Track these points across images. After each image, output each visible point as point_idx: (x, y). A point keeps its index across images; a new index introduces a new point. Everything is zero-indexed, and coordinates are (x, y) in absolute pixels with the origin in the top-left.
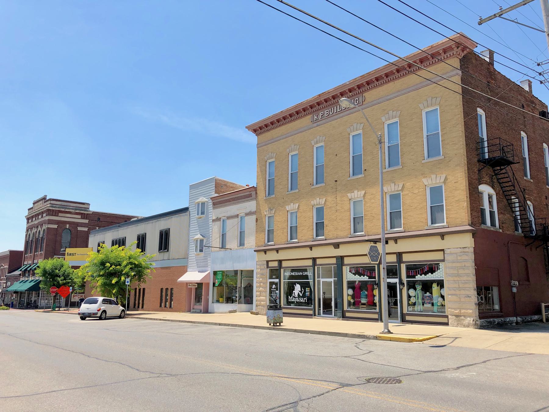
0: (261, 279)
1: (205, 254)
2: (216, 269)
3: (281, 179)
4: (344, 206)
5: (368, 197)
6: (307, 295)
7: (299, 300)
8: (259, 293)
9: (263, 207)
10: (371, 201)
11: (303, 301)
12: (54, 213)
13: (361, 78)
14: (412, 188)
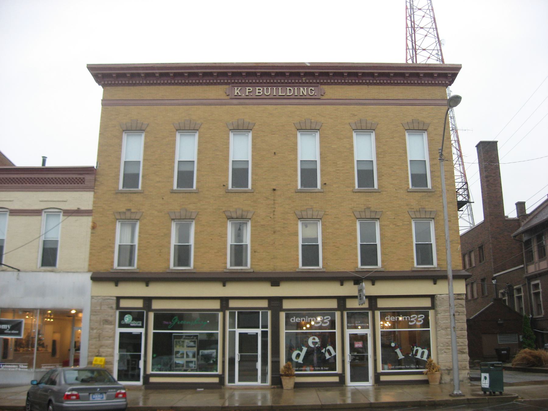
14: (394, 219)
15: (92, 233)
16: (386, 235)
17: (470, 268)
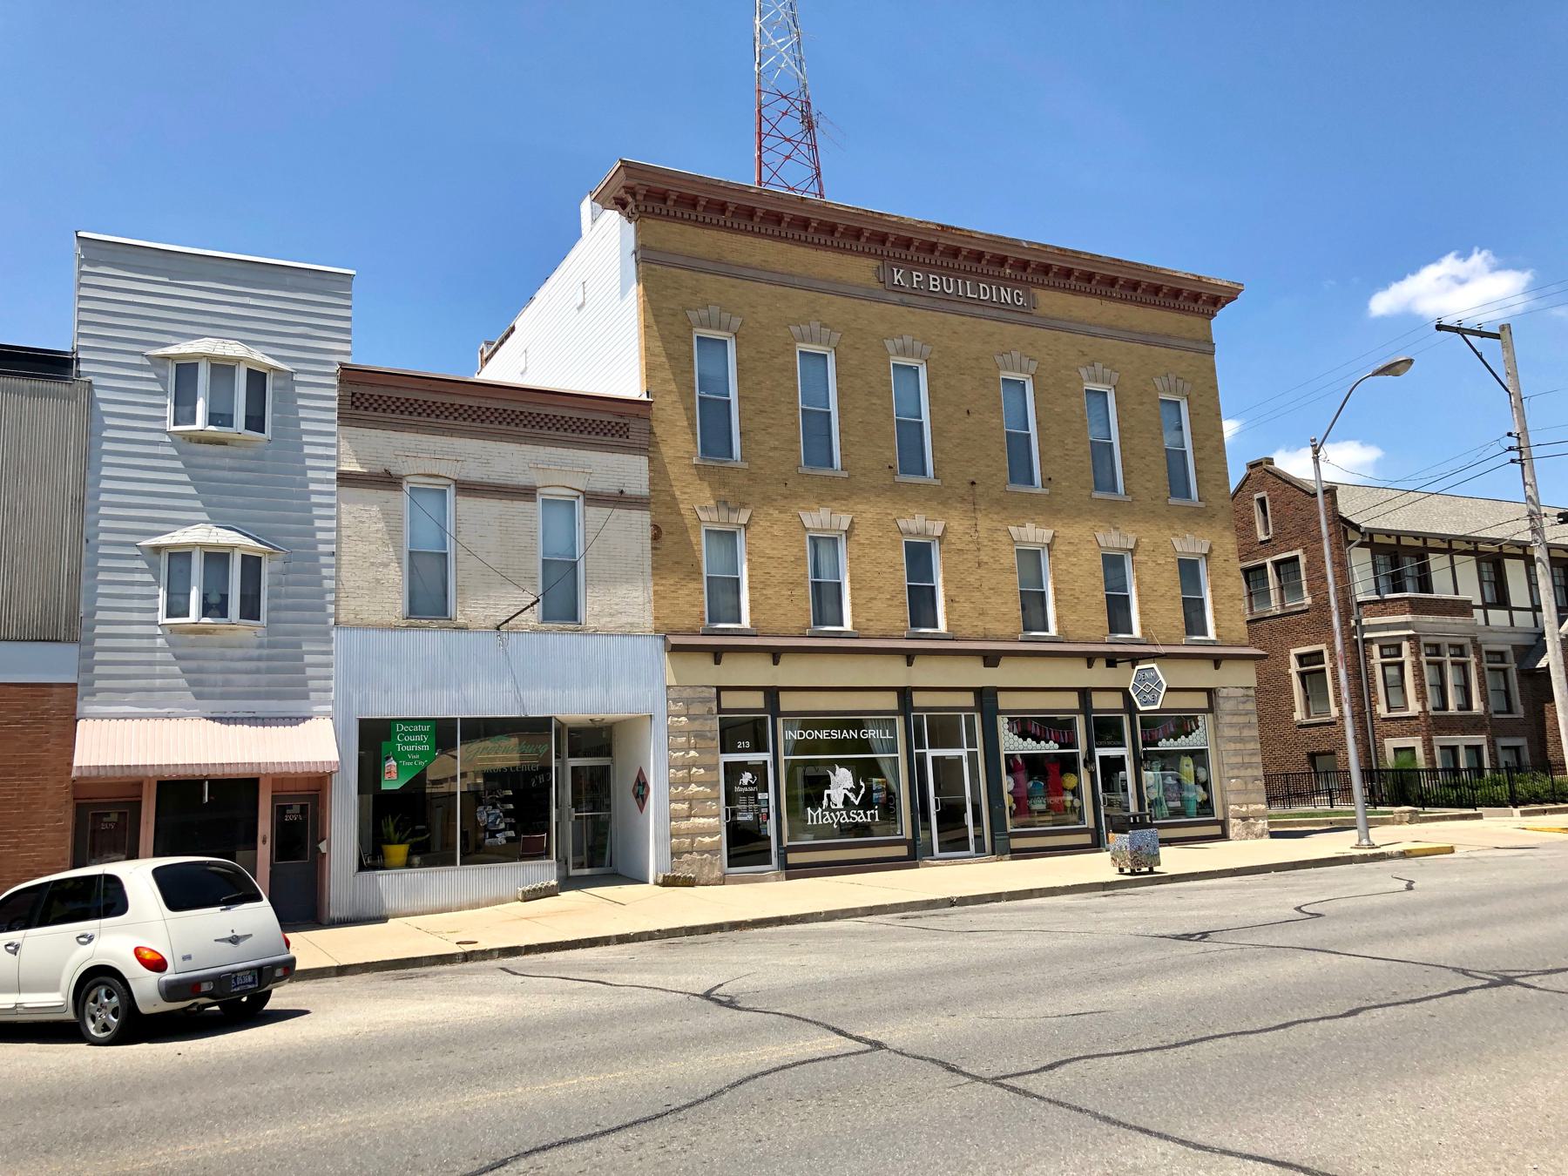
1: (270, 632)
4: (1001, 556)
5: (1062, 548)
7: (849, 817)
8: (686, 806)
10: (1070, 559)
12: (1318, 582)
14: (1153, 551)
15: (653, 548)
16: (1144, 580)
17: (404, 623)
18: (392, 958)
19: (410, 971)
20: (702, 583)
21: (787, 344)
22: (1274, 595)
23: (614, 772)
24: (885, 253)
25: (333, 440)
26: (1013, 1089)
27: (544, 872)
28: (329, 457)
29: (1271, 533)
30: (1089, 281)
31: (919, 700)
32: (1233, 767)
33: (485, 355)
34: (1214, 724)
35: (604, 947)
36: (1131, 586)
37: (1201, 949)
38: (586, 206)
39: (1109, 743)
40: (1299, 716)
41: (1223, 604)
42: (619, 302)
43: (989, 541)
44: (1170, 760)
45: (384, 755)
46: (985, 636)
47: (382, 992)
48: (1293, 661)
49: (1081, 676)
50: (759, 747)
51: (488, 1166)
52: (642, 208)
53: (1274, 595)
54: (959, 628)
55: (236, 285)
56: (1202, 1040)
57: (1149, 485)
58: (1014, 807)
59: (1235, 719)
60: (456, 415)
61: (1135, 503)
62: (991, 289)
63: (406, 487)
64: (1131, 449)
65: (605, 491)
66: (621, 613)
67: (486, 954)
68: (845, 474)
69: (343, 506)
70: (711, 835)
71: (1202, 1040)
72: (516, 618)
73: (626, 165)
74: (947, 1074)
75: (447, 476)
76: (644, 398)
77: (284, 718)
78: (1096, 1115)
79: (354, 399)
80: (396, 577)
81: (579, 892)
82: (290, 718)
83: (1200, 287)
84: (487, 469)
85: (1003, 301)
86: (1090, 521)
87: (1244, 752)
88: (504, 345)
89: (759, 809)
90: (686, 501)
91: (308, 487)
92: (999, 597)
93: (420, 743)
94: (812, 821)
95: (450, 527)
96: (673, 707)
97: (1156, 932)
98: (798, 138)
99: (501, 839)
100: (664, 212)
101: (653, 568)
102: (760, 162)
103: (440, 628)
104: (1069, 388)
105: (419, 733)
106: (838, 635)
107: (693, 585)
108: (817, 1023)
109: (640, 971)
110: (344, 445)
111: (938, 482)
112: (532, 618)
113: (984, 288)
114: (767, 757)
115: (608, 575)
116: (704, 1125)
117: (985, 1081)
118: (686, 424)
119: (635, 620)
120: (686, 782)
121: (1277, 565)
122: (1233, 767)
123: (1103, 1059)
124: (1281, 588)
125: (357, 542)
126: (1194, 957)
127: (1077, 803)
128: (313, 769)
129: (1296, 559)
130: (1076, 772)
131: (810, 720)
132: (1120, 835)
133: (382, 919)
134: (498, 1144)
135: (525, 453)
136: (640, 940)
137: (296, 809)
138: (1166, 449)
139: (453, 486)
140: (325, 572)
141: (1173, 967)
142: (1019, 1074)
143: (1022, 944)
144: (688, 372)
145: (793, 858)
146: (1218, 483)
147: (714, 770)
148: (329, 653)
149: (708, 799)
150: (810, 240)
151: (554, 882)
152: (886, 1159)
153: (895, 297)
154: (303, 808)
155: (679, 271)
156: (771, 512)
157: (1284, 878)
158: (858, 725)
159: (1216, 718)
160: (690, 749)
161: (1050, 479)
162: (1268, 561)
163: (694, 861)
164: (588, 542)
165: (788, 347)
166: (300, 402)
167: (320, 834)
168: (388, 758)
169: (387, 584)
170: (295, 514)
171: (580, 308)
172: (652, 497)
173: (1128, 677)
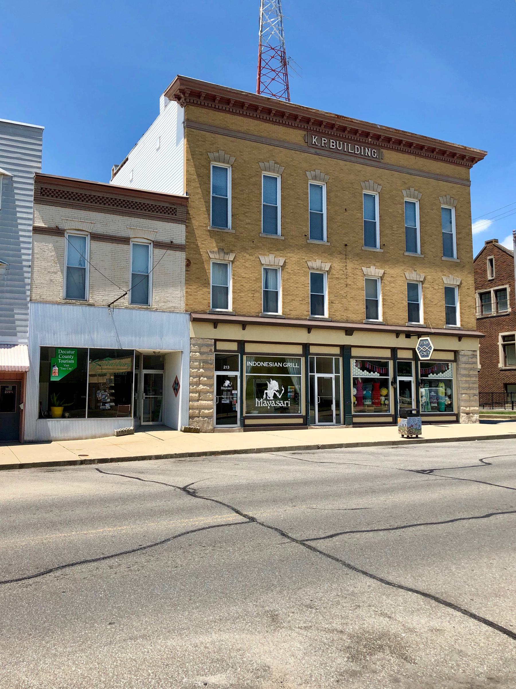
0: (201, 370)
2: (51, 342)
3: (248, 207)
5: (388, 279)
6: (289, 396)
7: (276, 404)
8: (197, 395)
9: (204, 242)
11: (283, 405)
13: (394, 131)
15: (186, 271)
18: (46, 461)
19: (54, 468)
20: (209, 289)
21: (257, 171)
22: (493, 306)
23: (165, 377)
24: (309, 128)
25: (31, 211)
26: (309, 547)
27: (128, 423)
28: (29, 219)
29: (494, 276)
30: (443, 154)
31: (313, 350)
32: (464, 388)
33: (114, 172)
34: (456, 368)
35: (148, 461)
36: (421, 299)
37: (427, 478)
38: (163, 99)
39: (404, 374)
40: (501, 365)
41: (465, 310)
42: (175, 147)
43: (352, 274)
44: (432, 383)
45: (52, 365)
46: (347, 320)
47: (35, 478)
48: (500, 339)
49: (391, 341)
50: (234, 368)
51: (42, 573)
52: (188, 101)
53: (493, 306)
54: (334, 316)
55: (7, 135)
56: (410, 526)
57: (433, 250)
58: (356, 402)
59: (467, 366)
60: (101, 202)
61: (425, 258)
62: (361, 148)
63: (66, 235)
64: (425, 232)
65: (163, 241)
66: (169, 301)
67: (91, 462)
68: (283, 238)
69: (35, 243)
70: (209, 409)
71: (410, 526)
72: (118, 301)
73: (180, 78)
74: (280, 537)
75: (87, 230)
76: (185, 196)
77: (4, 345)
78: (344, 564)
79: (42, 191)
80: (60, 278)
81: (144, 433)
82: (7, 345)
83: (464, 152)
84: (106, 228)
85: (366, 155)
86: (402, 266)
87: (470, 382)
88: (124, 167)
89: (233, 398)
90: (203, 248)
91: (18, 233)
92: (355, 302)
93: (70, 359)
94: (258, 405)
95: (87, 256)
96: (193, 348)
97: (409, 468)
98: (279, 70)
99: (108, 406)
100: (199, 103)
101: (186, 280)
102: (260, 81)
103: (81, 304)
104: (396, 200)
105: (69, 354)
106: (275, 317)
107: (205, 290)
108: (228, 506)
109: (159, 474)
110: (37, 214)
111: (329, 244)
112: (126, 301)
113: (357, 148)
114: (238, 374)
115: (163, 283)
116: (153, 557)
117: (297, 541)
118: (205, 209)
119: (177, 305)
120: (198, 384)
121: (496, 292)
122: (464, 388)
123: (358, 533)
124: (497, 303)
125: (42, 261)
126: (421, 483)
127: (387, 402)
128: (17, 370)
129: (505, 289)
130: (387, 388)
131: (260, 357)
132: (403, 419)
133: (49, 442)
134: (52, 561)
135: (125, 221)
136: (166, 458)
137: (10, 388)
138: (443, 233)
139: (89, 236)
140: (26, 275)
141: (409, 488)
142: (315, 539)
143: (343, 470)
144: (207, 184)
145: (248, 422)
146: (467, 250)
147: (211, 378)
148: (27, 314)
149: (208, 392)
150: (271, 119)
151: (132, 428)
152: (233, 581)
153: (313, 150)
154: (14, 388)
155: (205, 132)
156: (245, 255)
157: (480, 444)
158: (283, 361)
159: (457, 365)
160: (200, 368)
161: (384, 245)
162: (492, 290)
163: (200, 421)
164: (154, 266)
165: (258, 173)
166: (16, 191)
167: (21, 400)
168: (54, 366)
169: (55, 282)
170: (11, 246)
171: (158, 150)
172: (187, 245)
173: (416, 343)
